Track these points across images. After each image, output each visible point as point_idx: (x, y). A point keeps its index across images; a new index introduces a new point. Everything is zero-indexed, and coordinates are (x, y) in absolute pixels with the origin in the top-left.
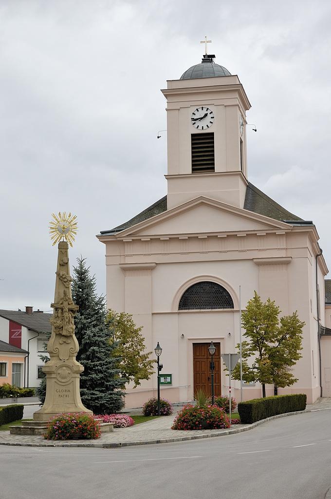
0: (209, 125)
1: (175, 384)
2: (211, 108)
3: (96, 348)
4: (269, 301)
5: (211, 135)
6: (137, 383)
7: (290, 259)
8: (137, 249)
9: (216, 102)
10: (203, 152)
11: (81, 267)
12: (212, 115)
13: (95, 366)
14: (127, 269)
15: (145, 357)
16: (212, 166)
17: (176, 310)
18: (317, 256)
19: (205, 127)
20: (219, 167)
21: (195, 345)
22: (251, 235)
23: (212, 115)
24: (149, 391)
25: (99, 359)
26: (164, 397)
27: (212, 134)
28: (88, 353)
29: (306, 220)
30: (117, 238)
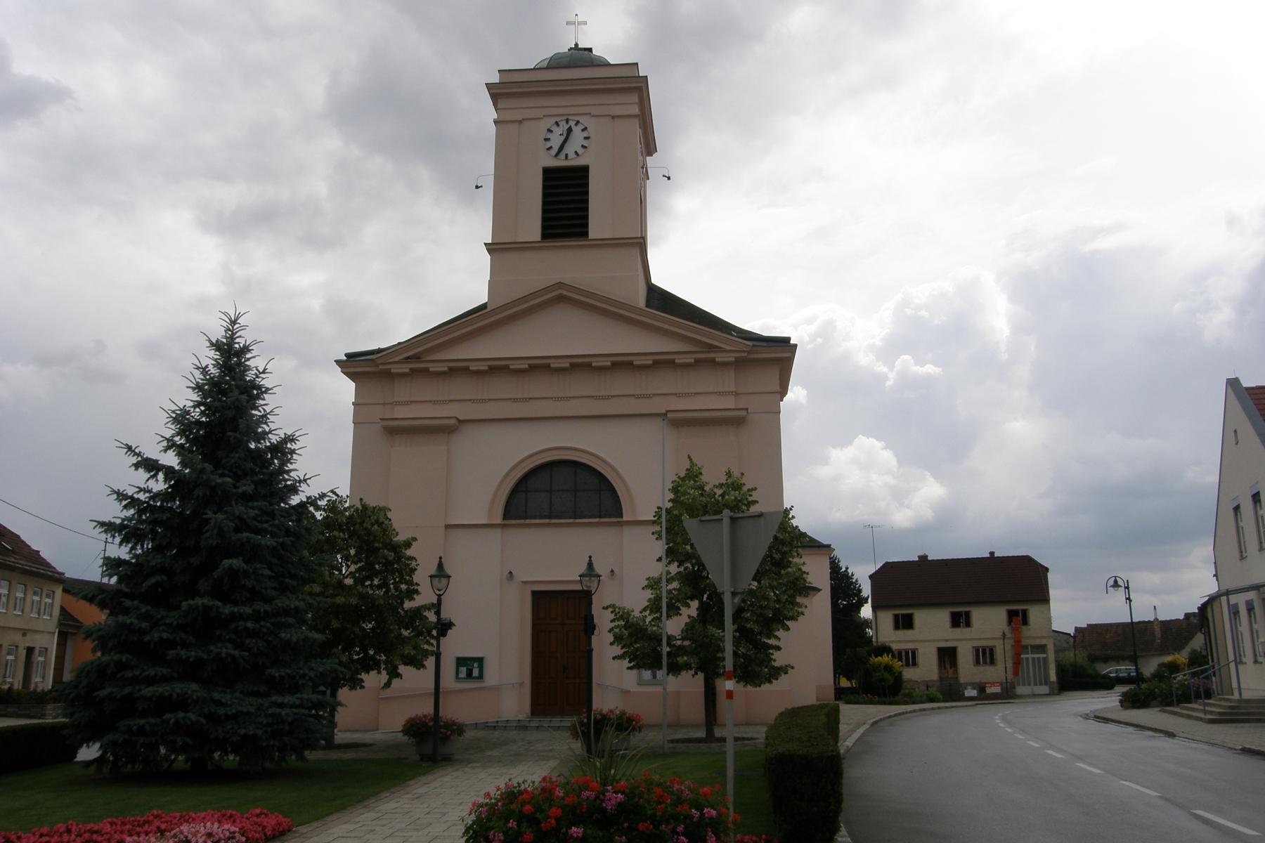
1: (491, 677)
2: (581, 119)
3: (236, 563)
4: (729, 474)
5: (583, 172)
6: (394, 674)
7: (744, 413)
8: (423, 389)
9: (594, 111)
11: (232, 338)
13: (234, 617)
14: (396, 431)
15: (417, 613)
17: (499, 520)
20: (593, 234)
21: (537, 595)
22: (662, 364)
25: (255, 595)
26: (453, 711)
28: (216, 575)
30: (377, 365)
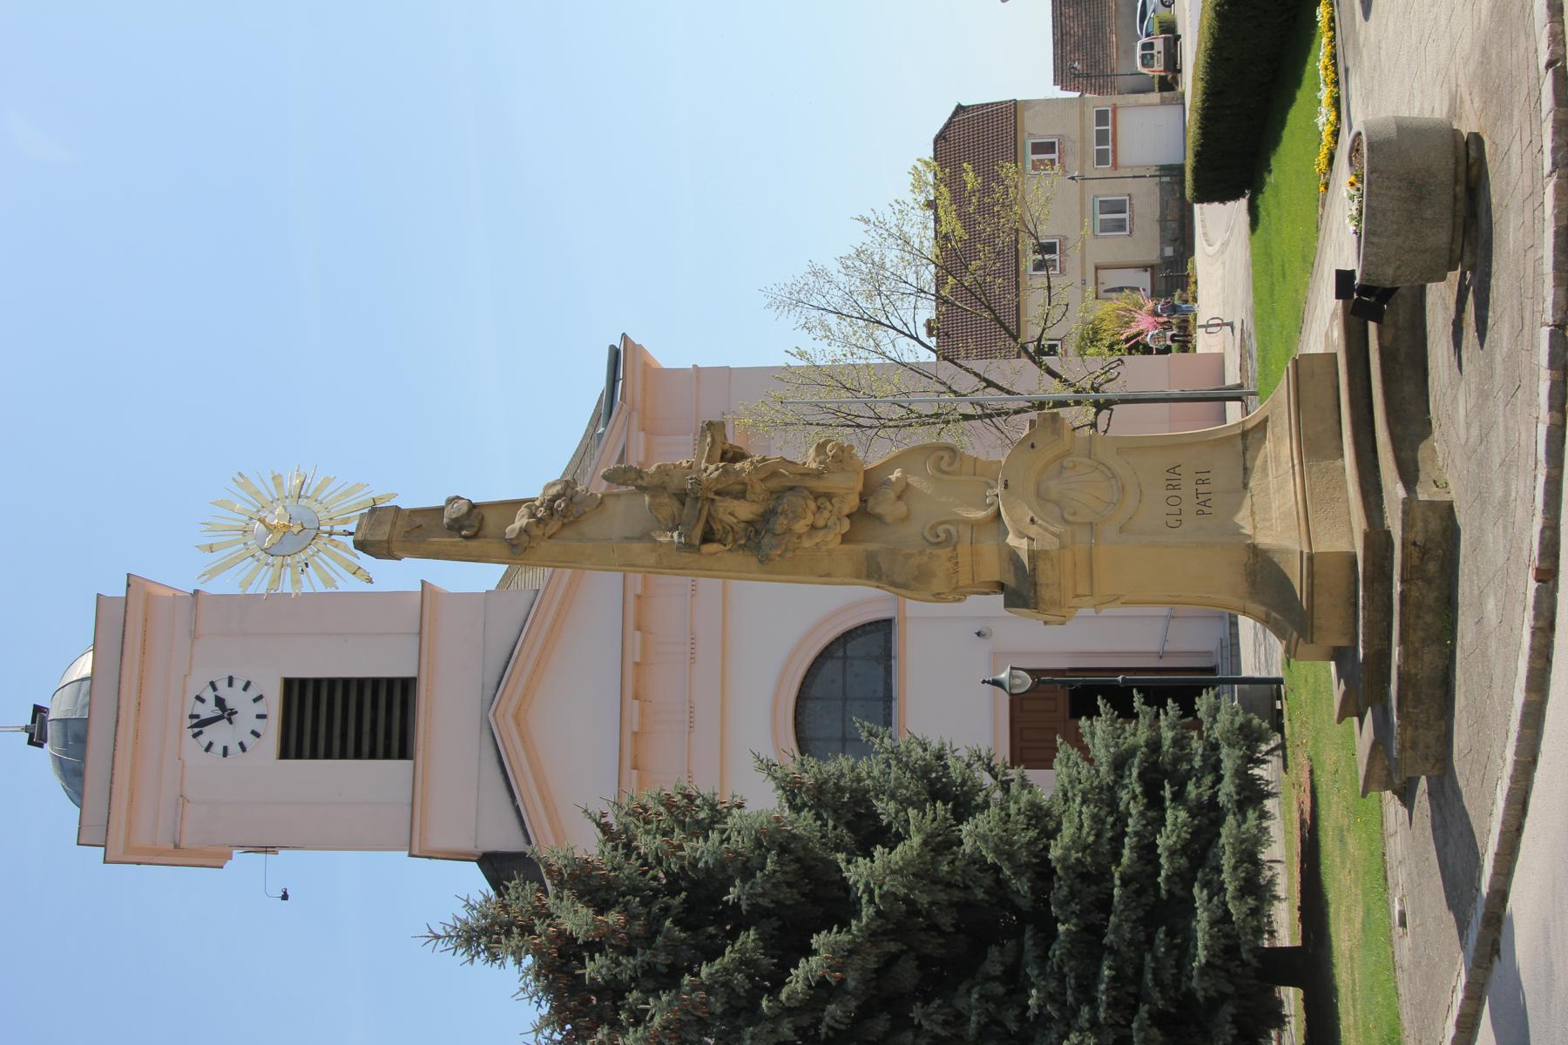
0: (253, 692)
10: (348, 718)
16: (366, 748)
19: (260, 708)
23: (222, 686)
27: (288, 683)
29: (601, 383)
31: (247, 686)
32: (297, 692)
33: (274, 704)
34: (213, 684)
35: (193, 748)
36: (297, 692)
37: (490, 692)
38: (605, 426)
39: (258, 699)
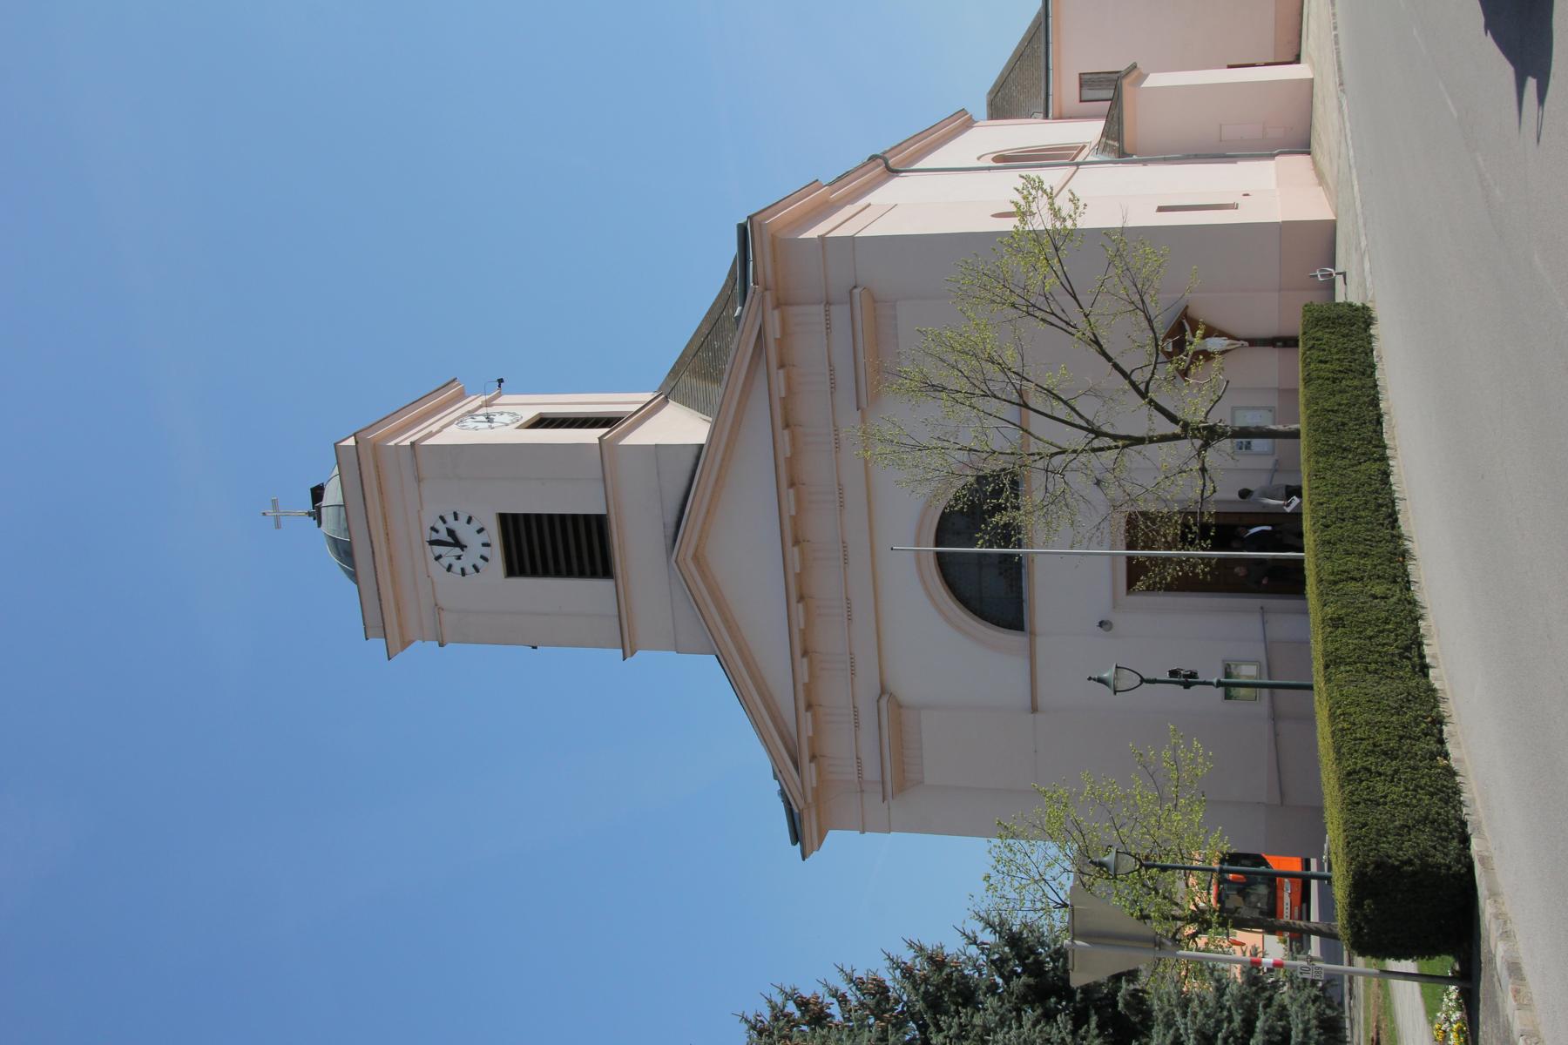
0: (475, 525)
12: (450, 519)
18: (893, 172)
19: (483, 538)
20: (595, 508)
23: (450, 519)
24: (1276, 735)
29: (733, 249)
31: (469, 520)
32: (511, 524)
33: (494, 534)
34: (442, 518)
35: (437, 569)
36: (511, 524)
37: (671, 530)
38: (743, 305)
39: (480, 531)
